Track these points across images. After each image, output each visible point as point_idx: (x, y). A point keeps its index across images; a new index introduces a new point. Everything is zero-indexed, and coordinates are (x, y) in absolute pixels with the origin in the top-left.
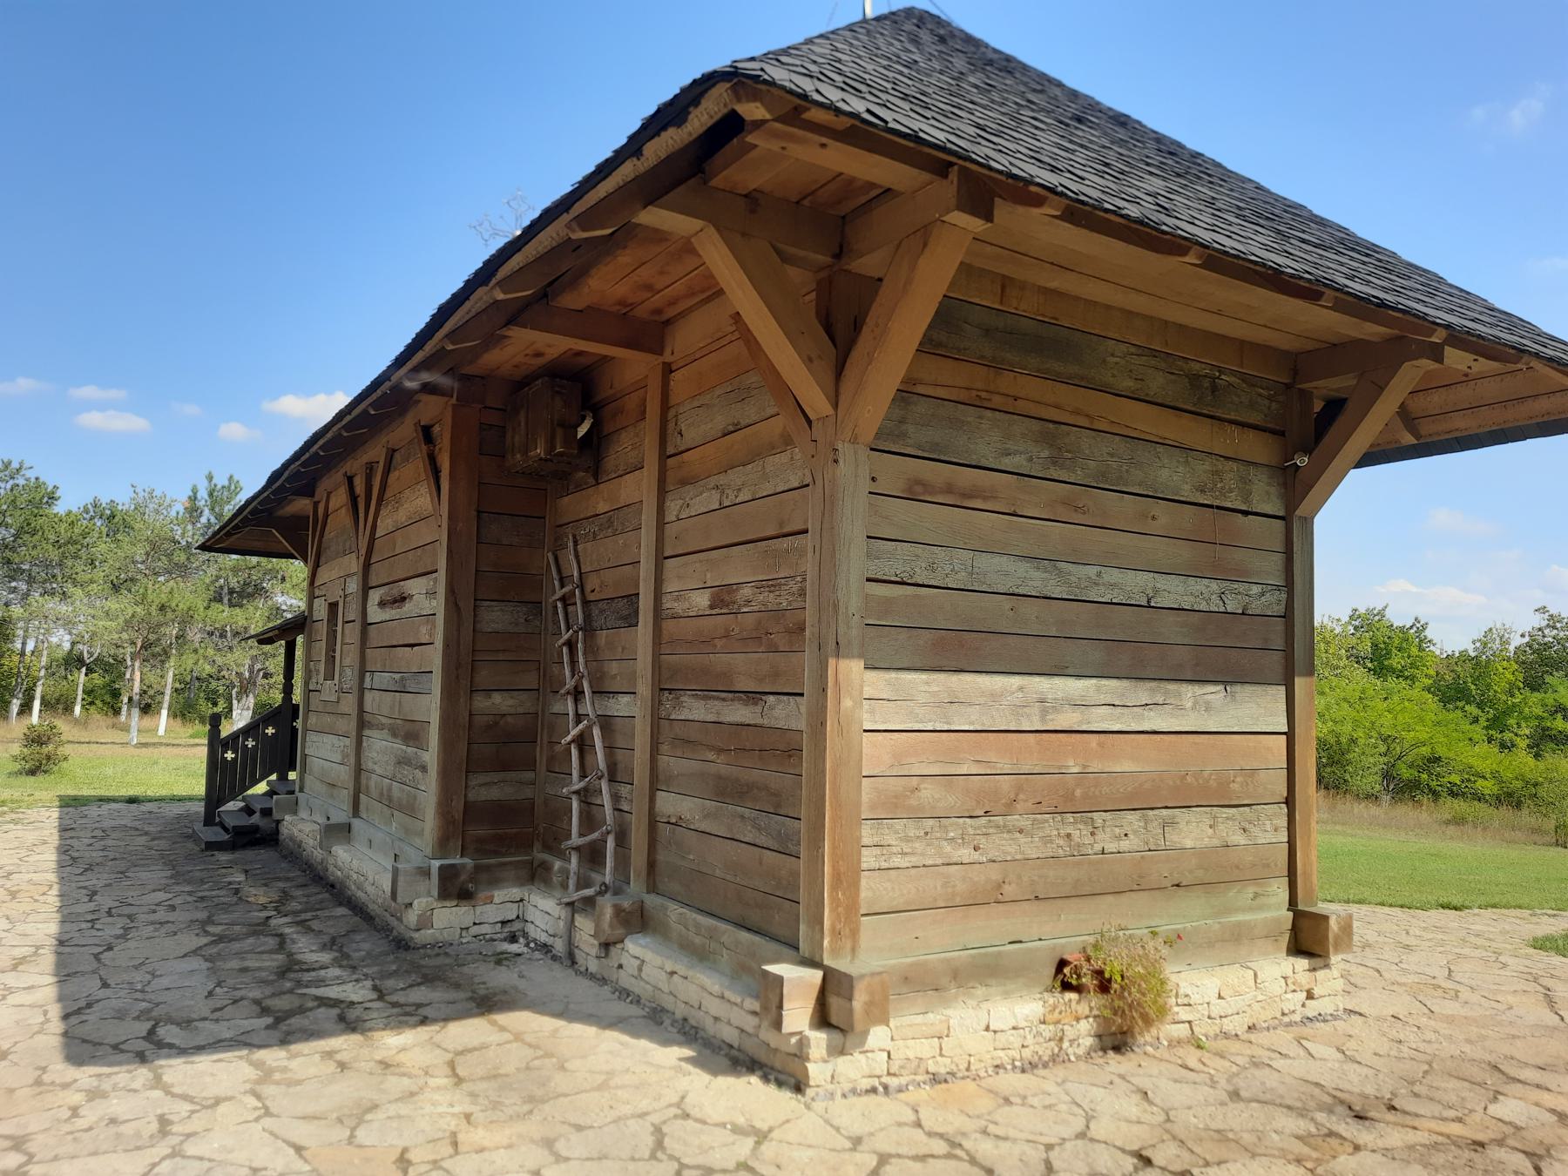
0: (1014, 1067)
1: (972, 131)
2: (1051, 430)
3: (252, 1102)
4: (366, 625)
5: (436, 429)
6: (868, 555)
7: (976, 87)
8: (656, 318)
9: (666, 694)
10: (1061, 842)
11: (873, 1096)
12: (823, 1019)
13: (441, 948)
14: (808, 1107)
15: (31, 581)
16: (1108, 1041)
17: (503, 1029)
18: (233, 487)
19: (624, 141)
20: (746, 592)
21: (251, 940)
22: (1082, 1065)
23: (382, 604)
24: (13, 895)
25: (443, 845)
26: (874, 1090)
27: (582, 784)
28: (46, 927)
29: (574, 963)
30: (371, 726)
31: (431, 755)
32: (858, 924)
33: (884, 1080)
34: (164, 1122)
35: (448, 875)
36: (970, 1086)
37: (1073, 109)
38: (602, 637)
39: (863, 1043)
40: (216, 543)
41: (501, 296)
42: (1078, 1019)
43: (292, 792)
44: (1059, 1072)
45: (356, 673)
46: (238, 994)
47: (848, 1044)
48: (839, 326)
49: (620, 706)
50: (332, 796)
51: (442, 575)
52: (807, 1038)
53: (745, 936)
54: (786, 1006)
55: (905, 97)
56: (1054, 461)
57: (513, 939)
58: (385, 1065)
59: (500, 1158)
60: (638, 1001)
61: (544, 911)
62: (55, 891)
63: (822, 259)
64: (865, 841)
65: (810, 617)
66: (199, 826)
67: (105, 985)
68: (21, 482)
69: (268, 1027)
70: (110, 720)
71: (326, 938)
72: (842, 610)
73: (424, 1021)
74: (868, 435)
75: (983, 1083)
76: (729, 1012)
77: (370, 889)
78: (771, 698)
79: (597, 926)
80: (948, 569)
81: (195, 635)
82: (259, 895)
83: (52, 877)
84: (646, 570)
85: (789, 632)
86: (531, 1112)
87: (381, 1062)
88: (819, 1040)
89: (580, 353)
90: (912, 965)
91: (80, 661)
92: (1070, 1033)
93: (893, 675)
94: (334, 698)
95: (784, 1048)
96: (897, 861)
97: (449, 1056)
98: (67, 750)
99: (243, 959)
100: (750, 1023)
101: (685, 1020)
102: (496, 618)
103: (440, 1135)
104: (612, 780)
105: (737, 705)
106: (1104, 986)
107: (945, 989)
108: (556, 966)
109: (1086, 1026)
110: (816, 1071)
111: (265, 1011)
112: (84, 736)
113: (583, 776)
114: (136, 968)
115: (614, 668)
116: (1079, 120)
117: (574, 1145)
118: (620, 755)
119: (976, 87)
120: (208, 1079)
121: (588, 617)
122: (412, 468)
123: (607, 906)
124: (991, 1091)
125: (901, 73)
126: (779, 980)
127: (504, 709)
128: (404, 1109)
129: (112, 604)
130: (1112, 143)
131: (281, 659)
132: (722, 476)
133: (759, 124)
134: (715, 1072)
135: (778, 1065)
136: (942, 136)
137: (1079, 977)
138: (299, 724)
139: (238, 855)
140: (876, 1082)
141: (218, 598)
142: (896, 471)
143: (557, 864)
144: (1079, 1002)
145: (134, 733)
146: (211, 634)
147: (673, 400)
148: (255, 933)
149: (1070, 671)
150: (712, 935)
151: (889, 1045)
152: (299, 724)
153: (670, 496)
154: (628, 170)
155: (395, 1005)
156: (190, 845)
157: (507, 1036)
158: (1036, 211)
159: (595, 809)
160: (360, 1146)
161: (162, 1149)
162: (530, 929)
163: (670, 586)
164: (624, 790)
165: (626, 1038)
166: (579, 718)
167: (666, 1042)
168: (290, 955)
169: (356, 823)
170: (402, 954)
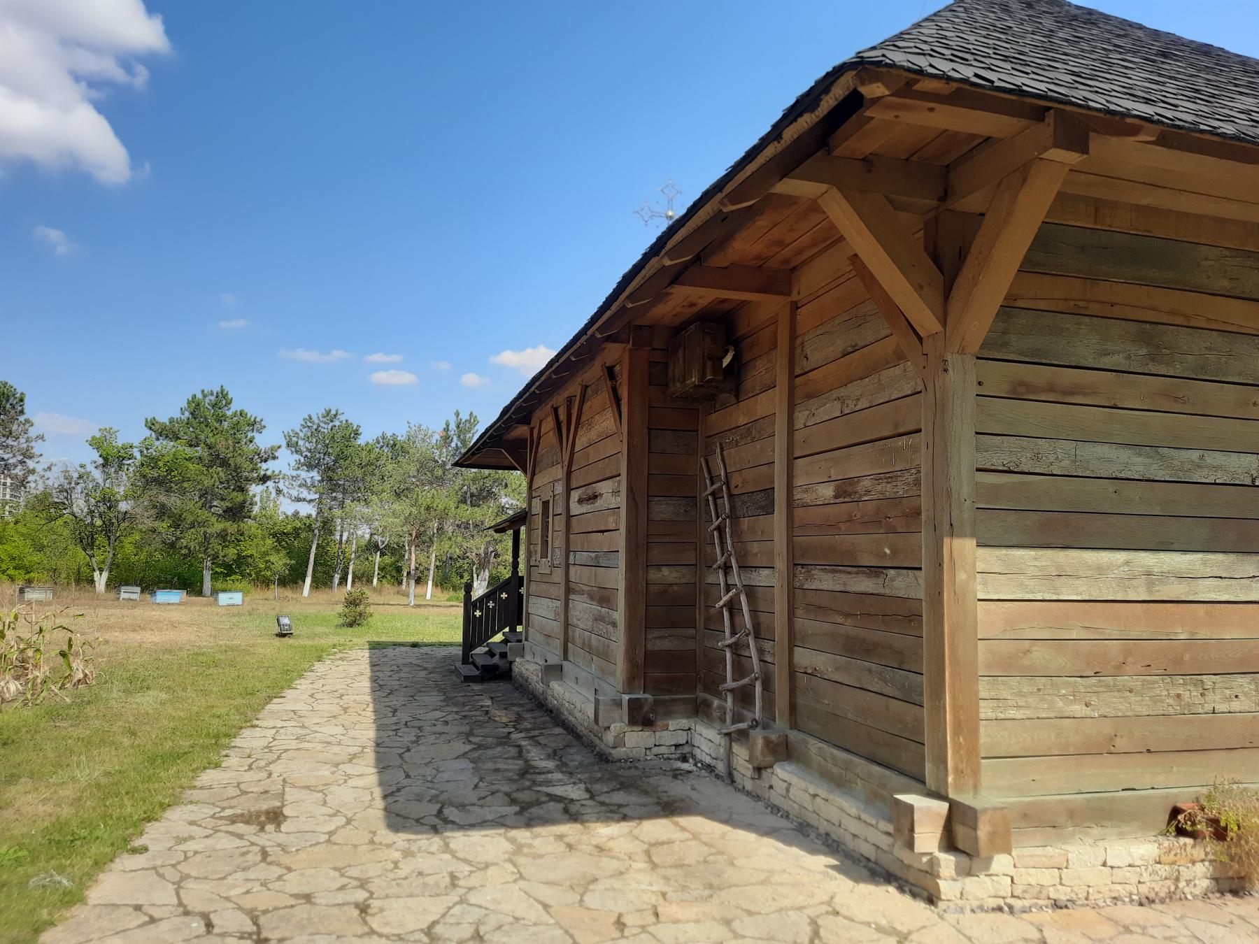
0: (1132, 901)
1: (1069, 78)
2: (1148, 332)
3: (510, 868)
4: (569, 517)
5: (617, 368)
6: (978, 449)
7: (1067, 40)
9: (799, 568)
10: (1171, 701)
11: (999, 914)
12: (950, 843)
13: (631, 762)
14: (942, 918)
15: (345, 492)
16: (1226, 886)
17: (683, 829)
18: (472, 421)
19: (769, 129)
20: (866, 483)
21: (499, 749)
22: (1200, 904)
23: (580, 501)
24: (345, 710)
25: (630, 683)
26: (1000, 909)
27: (733, 640)
28: (367, 733)
29: (733, 781)
30: (575, 592)
31: (619, 615)
32: (979, 764)
33: (1009, 901)
34: (453, 877)
35: (634, 706)
36: (1091, 914)
37: (1157, 46)
38: (745, 523)
39: (987, 867)
40: (465, 461)
41: (668, 263)
42: (1194, 862)
43: (520, 641)
44: (1177, 908)
45: (563, 552)
46: (495, 788)
47: (974, 867)
48: (946, 258)
49: (761, 578)
50: (548, 644)
51: (624, 478)
52: (938, 859)
53: (875, 769)
54: (917, 829)
55: (1006, 59)
56: (1153, 358)
57: (684, 759)
58: (600, 849)
59: (691, 929)
60: (787, 816)
61: (708, 740)
62: (371, 708)
63: (930, 202)
64: (982, 694)
65: (925, 503)
66: (459, 664)
67: (408, 776)
68: (337, 423)
69: (516, 814)
70: (396, 589)
71: (550, 751)
72: (955, 496)
73: (625, 818)
74: (975, 347)
75: (1102, 912)
76: (870, 834)
77: (578, 715)
78: (892, 572)
79: (751, 753)
80: (1052, 458)
81: (449, 529)
82: (502, 716)
83: (368, 698)
85: (906, 516)
86: (711, 896)
87: (597, 847)
88: (947, 862)
89: (724, 301)
90: (1029, 803)
91: (376, 547)
92: (1186, 873)
93: (1004, 551)
94: (548, 571)
95: (916, 865)
96: (1012, 713)
97: (646, 846)
98: (371, 609)
99: (495, 763)
100: (885, 842)
101: (828, 834)
102: (664, 510)
103: (645, 906)
104: (757, 637)
105: (861, 577)
106: (1220, 833)
107: (1061, 827)
108: (719, 782)
109: (1201, 869)
110: (947, 887)
111: (513, 802)
112: (380, 600)
113: (733, 633)
114: (426, 764)
115: (755, 548)
116: (1164, 55)
117: (747, 926)
118: (763, 617)
119: (1067, 40)
120: (480, 849)
121: (732, 507)
122: (602, 398)
123: (758, 737)
124: (1111, 920)
125: (999, 39)
126: (910, 809)
127: (671, 580)
128: (617, 884)
129: (396, 506)
130: (1199, 71)
131: (510, 544)
132: (842, 389)
133: (876, 101)
134: (857, 880)
135: (911, 879)
136: (1042, 86)
137: (1194, 824)
138: (523, 590)
139: (486, 686)
140: (1001, 902)
141: (464, 501)
142: (999, 375)
143: (716, 702)
144: (1194, 846)
145: (412, 598)
146: (459, 526)
147: (799, 331)
148: (501, 744)
149: (1176, 547)
150: (847, 767)
151: (1012, 872)
152: (523, 590)
153: (798, 408)
154: (770, 151)
155: (602, 804)
156: (454, 678)
157: (687, 835)
158: (1130, 140)
159: (744, 660)
160: (588, 909)
161: (454, 897)
162: (697, 752)
163: (799, 481)
164: (767, 645)
165: (781, 845)
166: (728, 588)
167: (813, 852)
168: (527, 761)
169: (565, 664)
170: (604, 766)
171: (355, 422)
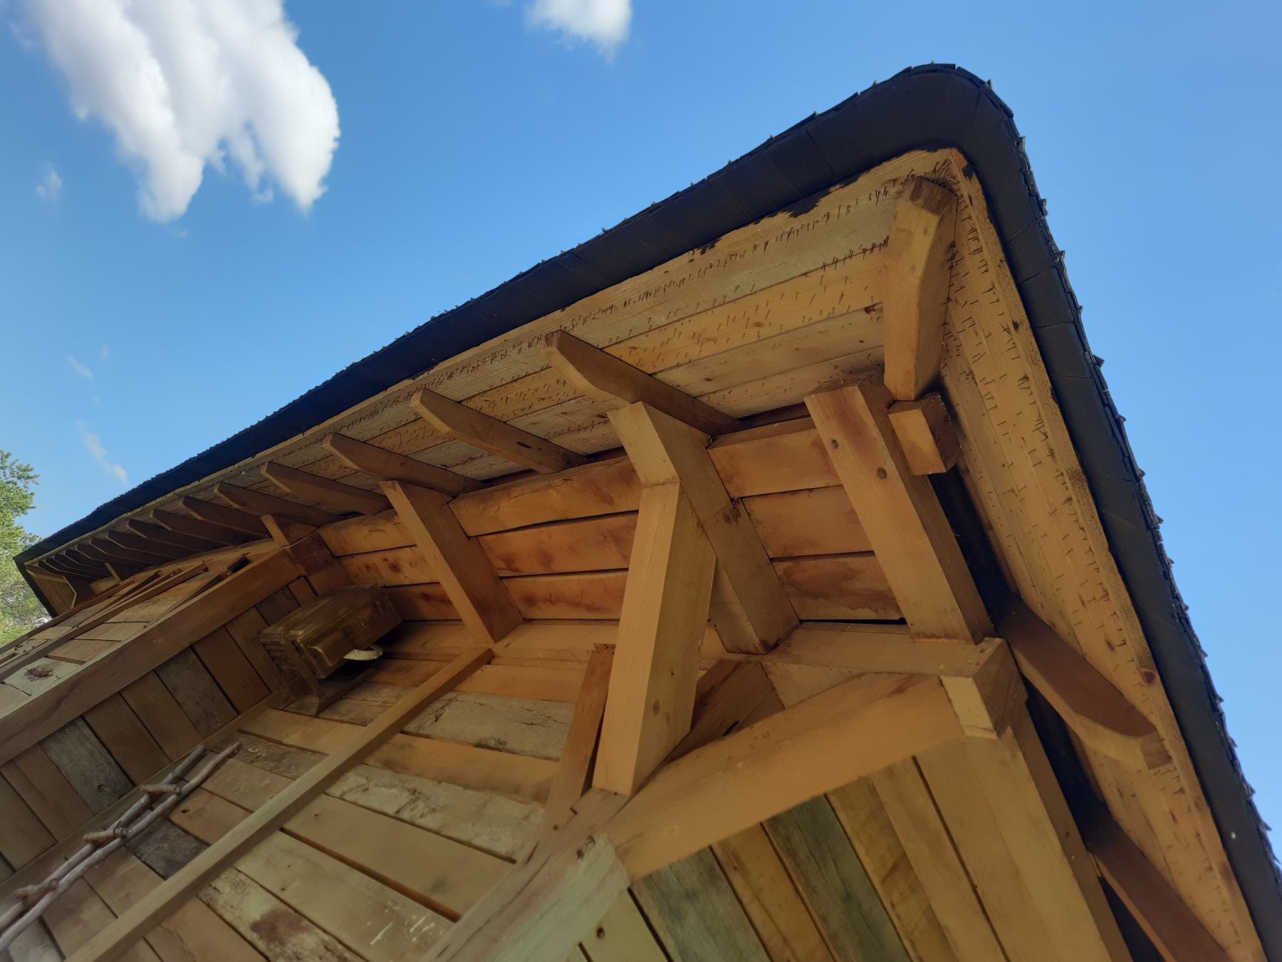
8: (523, 608)
48: (715, 711)
84: (246, 826)
102: (78, 756)
147: (465, 686)
153: (361, 769)
171: (35, 501)
